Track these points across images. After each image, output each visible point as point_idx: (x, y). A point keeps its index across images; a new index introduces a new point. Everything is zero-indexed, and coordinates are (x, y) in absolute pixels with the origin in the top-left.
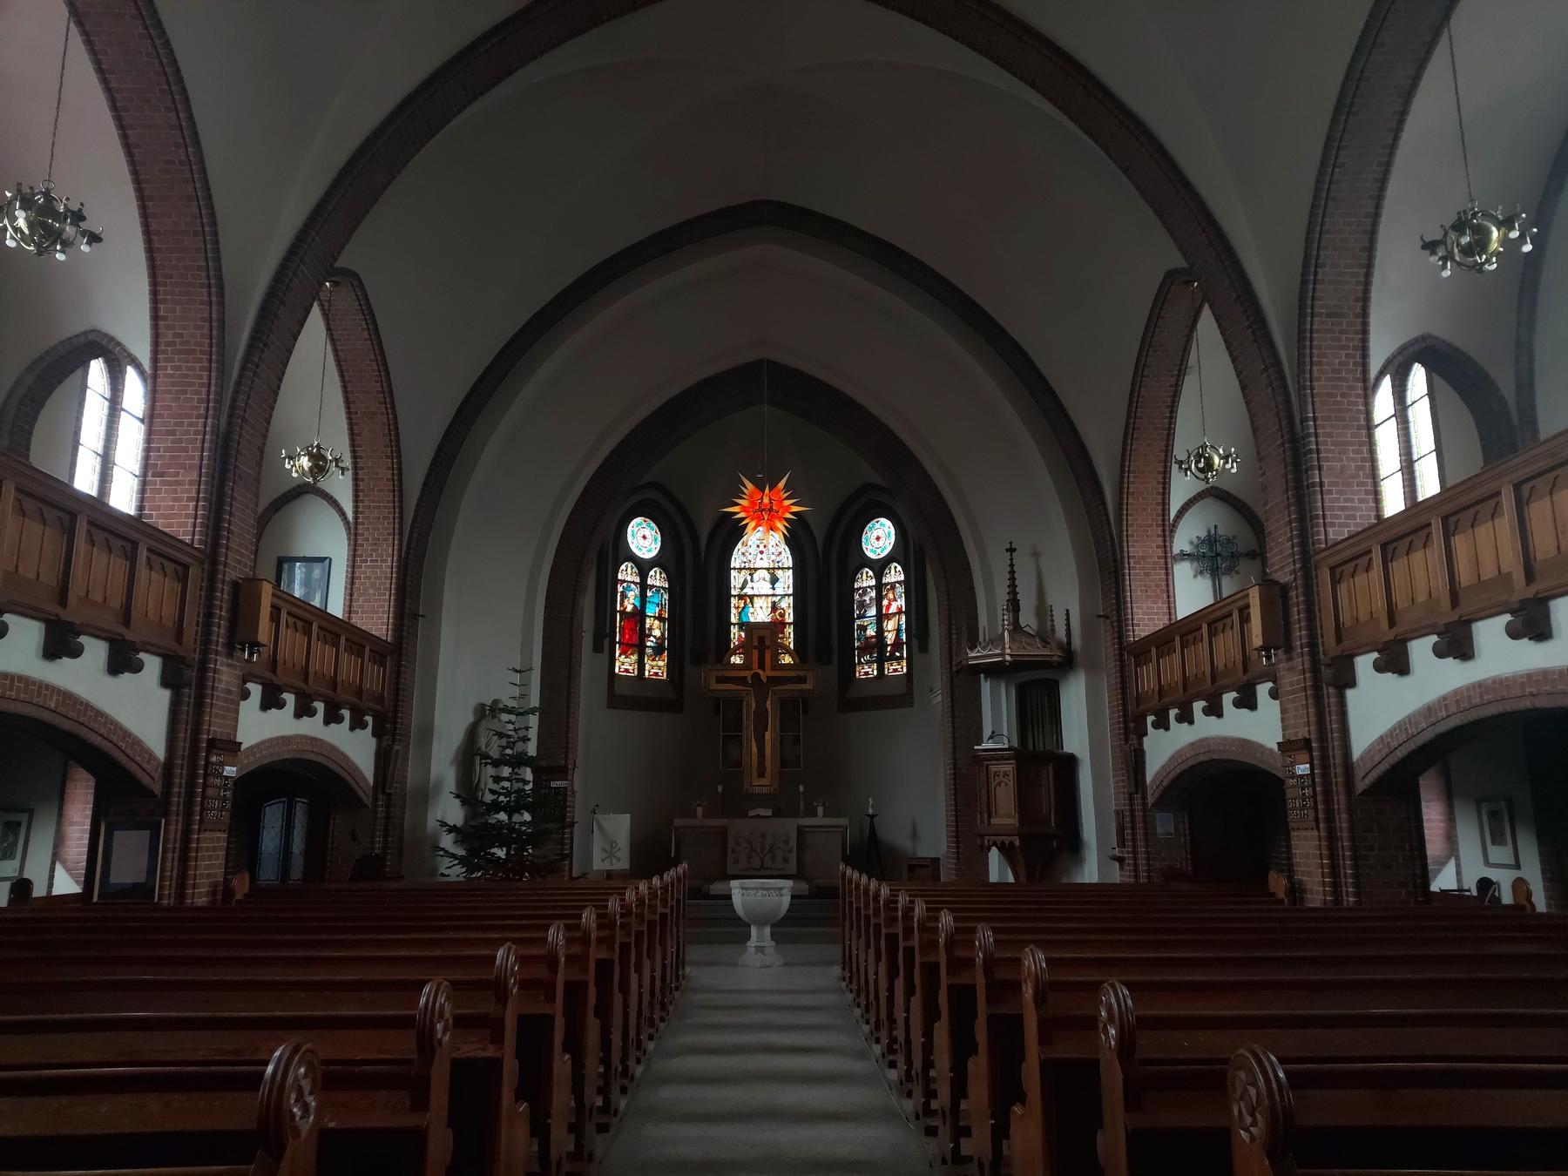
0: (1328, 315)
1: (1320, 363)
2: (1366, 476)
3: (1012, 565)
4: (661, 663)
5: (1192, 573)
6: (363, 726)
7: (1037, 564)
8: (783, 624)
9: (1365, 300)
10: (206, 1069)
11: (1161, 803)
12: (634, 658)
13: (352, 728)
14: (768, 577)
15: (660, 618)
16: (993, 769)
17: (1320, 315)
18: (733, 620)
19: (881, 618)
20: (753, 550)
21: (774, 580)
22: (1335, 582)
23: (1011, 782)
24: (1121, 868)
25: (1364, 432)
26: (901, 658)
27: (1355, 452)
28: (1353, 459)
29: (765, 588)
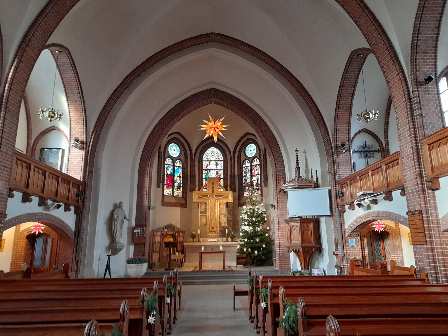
0: (423, 53)
1: (419, 71)
2: (438, 112)
3: (297, 156)
4: (180, 192)
5: (358, 157)
6: (69, 210)
7: (305, 155)
8: (220, 179)
9: (436, 47)
10: (100, 296)
11: (352, 234)
12: (171, 189)
13: (65, 211)
14: (215, 163)
15: (179, 177)
16: (292, 224)
17: (419, 53)
18: (204, 177)
19: (252, 176)
20: (210, 155)
21: (217, 164)
22: (430, 150)
23: (299, 228)
24: (337, 258)
25: (436, 96)
26: (259, 189)
27: (434, 103)
28: (433, 105)
29: (214, 167)
